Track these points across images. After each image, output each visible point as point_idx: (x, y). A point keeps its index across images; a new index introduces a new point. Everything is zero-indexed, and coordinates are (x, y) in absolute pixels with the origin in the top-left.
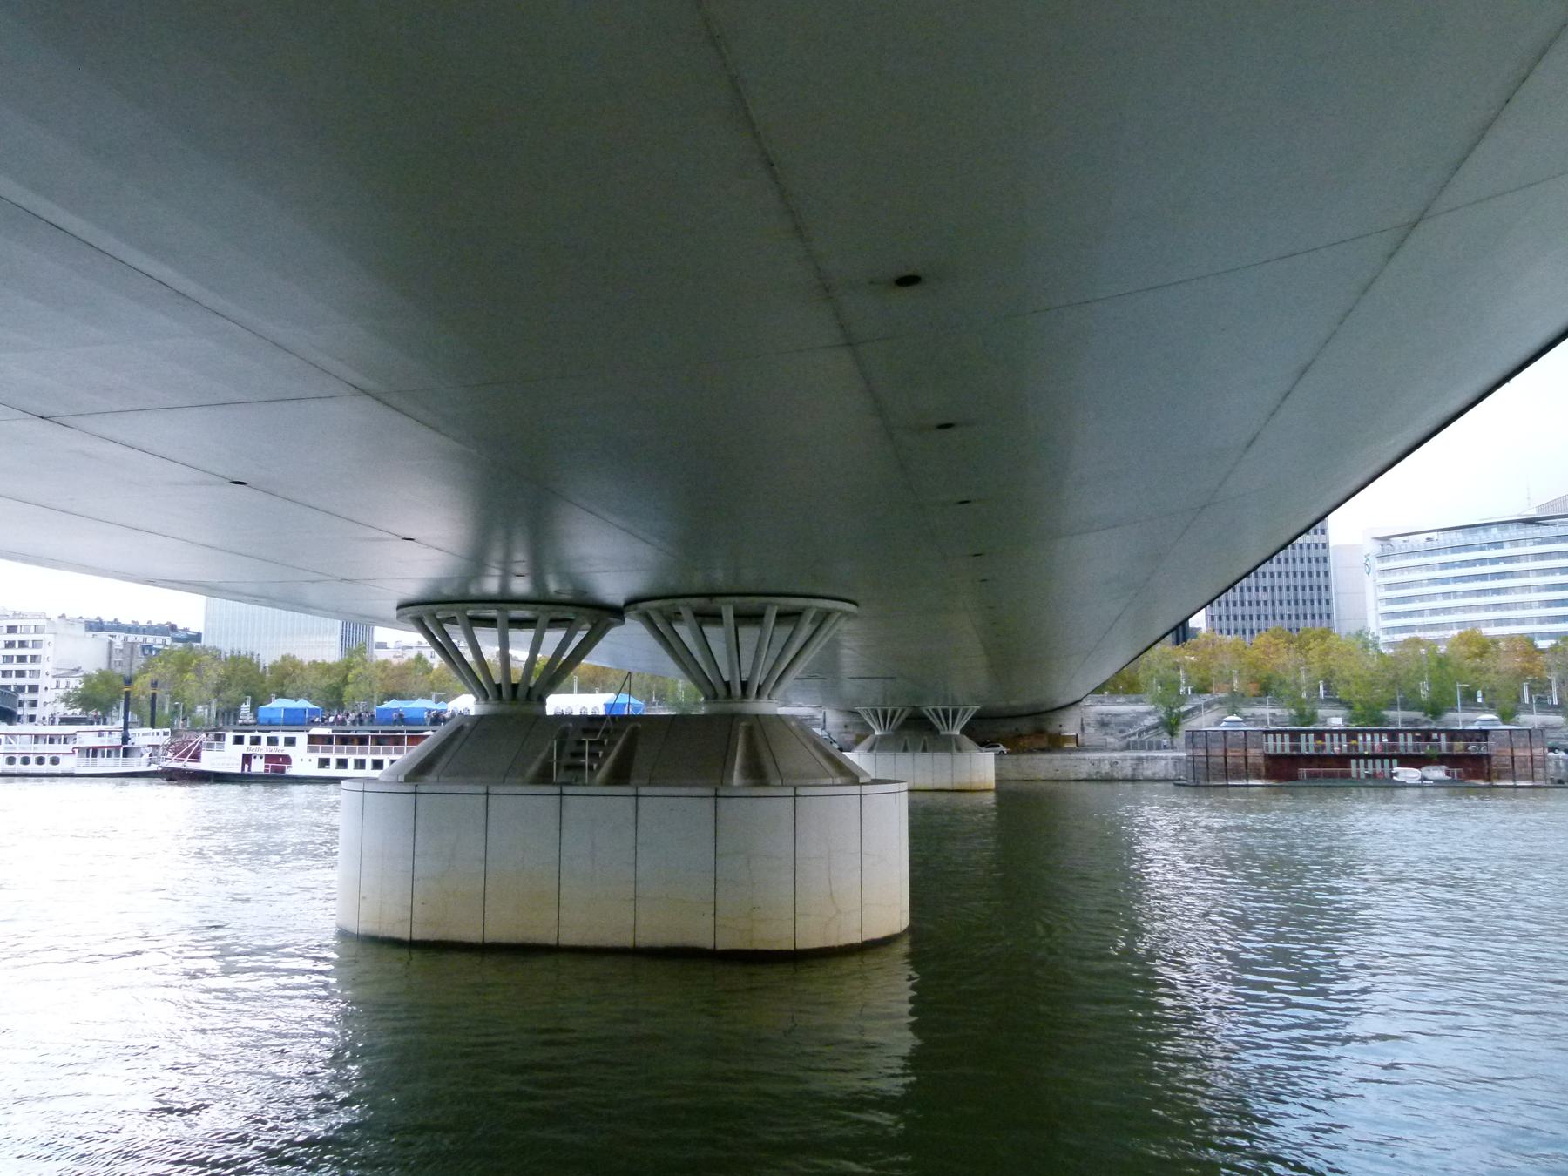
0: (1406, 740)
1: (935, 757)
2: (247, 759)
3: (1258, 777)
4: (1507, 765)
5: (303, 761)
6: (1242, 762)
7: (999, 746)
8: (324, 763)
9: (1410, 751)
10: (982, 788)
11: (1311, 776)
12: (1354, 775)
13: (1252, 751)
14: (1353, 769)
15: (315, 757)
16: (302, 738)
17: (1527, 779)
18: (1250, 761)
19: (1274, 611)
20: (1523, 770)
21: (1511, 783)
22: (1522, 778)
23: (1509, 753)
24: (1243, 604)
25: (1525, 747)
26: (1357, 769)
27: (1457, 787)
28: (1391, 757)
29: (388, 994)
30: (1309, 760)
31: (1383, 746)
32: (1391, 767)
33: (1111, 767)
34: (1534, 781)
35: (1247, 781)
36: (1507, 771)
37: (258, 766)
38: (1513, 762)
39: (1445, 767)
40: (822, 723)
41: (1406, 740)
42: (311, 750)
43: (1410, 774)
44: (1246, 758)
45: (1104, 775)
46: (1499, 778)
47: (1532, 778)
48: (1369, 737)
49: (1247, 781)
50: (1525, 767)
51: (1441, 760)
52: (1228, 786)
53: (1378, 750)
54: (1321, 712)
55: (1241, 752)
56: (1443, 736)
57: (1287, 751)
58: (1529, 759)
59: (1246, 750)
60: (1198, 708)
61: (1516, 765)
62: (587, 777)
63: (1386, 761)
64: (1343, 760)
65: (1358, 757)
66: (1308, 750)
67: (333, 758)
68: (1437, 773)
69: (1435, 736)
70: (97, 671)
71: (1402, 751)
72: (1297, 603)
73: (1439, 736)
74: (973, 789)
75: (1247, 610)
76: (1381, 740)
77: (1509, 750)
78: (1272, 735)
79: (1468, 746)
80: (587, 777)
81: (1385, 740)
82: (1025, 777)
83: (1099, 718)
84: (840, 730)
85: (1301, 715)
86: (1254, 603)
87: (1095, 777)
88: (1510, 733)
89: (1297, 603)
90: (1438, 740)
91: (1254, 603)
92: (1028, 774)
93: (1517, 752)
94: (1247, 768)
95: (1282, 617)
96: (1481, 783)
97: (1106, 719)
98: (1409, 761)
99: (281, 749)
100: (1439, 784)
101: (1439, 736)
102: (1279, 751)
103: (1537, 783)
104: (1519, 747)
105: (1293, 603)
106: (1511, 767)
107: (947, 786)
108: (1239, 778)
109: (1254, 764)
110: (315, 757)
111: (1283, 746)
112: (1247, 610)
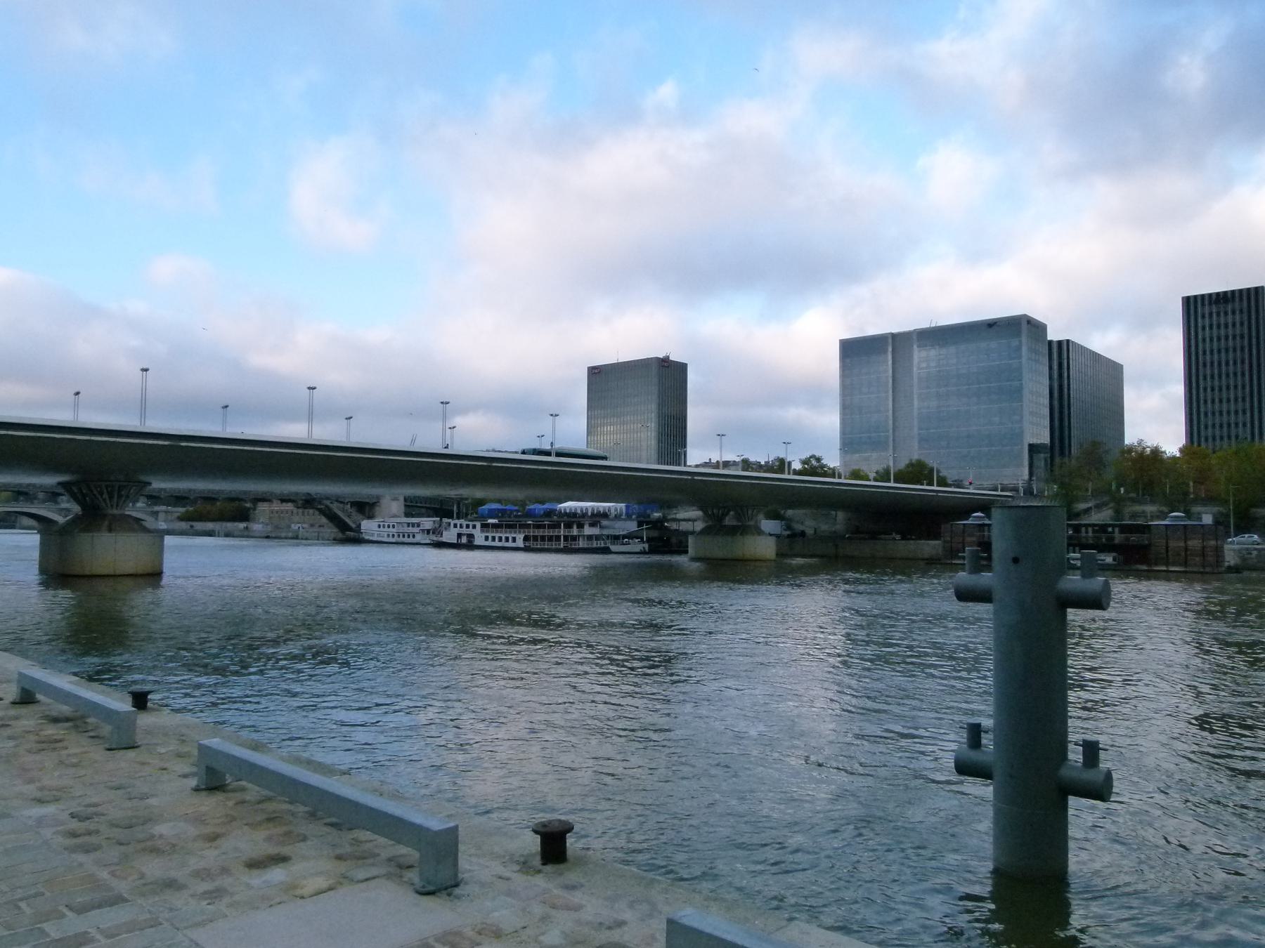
0: (1087, 532)
2: (459, 536)
5: (479, 539)
8: (487, 538)
10: (112, 572)
15: (484, 535)
16: (478, 525)
17: (1180, 565)
21: (1164, 568)
22: (1174, 564)
29: (560, 788)
37: (464, 540)
38: (1167, 551)
39: (1114, 554)
42: (482, 531)
46: (1156, 564)
47: (1185, 564)
50: (1179, 555)
52: (952, 564)
56: (1117, 530)
61: (1170, 553)
62: (1232, 530)
67: (490, 535)
70: (1152, 451)
74: (118, 572)
80: (1232, 530)
88: (1166, 529)
90: (1113, 532)
93: (1172, 544)
96: (1145, 568)
99: (470, 531)
101: (1113, 529)
110: (484, 535)
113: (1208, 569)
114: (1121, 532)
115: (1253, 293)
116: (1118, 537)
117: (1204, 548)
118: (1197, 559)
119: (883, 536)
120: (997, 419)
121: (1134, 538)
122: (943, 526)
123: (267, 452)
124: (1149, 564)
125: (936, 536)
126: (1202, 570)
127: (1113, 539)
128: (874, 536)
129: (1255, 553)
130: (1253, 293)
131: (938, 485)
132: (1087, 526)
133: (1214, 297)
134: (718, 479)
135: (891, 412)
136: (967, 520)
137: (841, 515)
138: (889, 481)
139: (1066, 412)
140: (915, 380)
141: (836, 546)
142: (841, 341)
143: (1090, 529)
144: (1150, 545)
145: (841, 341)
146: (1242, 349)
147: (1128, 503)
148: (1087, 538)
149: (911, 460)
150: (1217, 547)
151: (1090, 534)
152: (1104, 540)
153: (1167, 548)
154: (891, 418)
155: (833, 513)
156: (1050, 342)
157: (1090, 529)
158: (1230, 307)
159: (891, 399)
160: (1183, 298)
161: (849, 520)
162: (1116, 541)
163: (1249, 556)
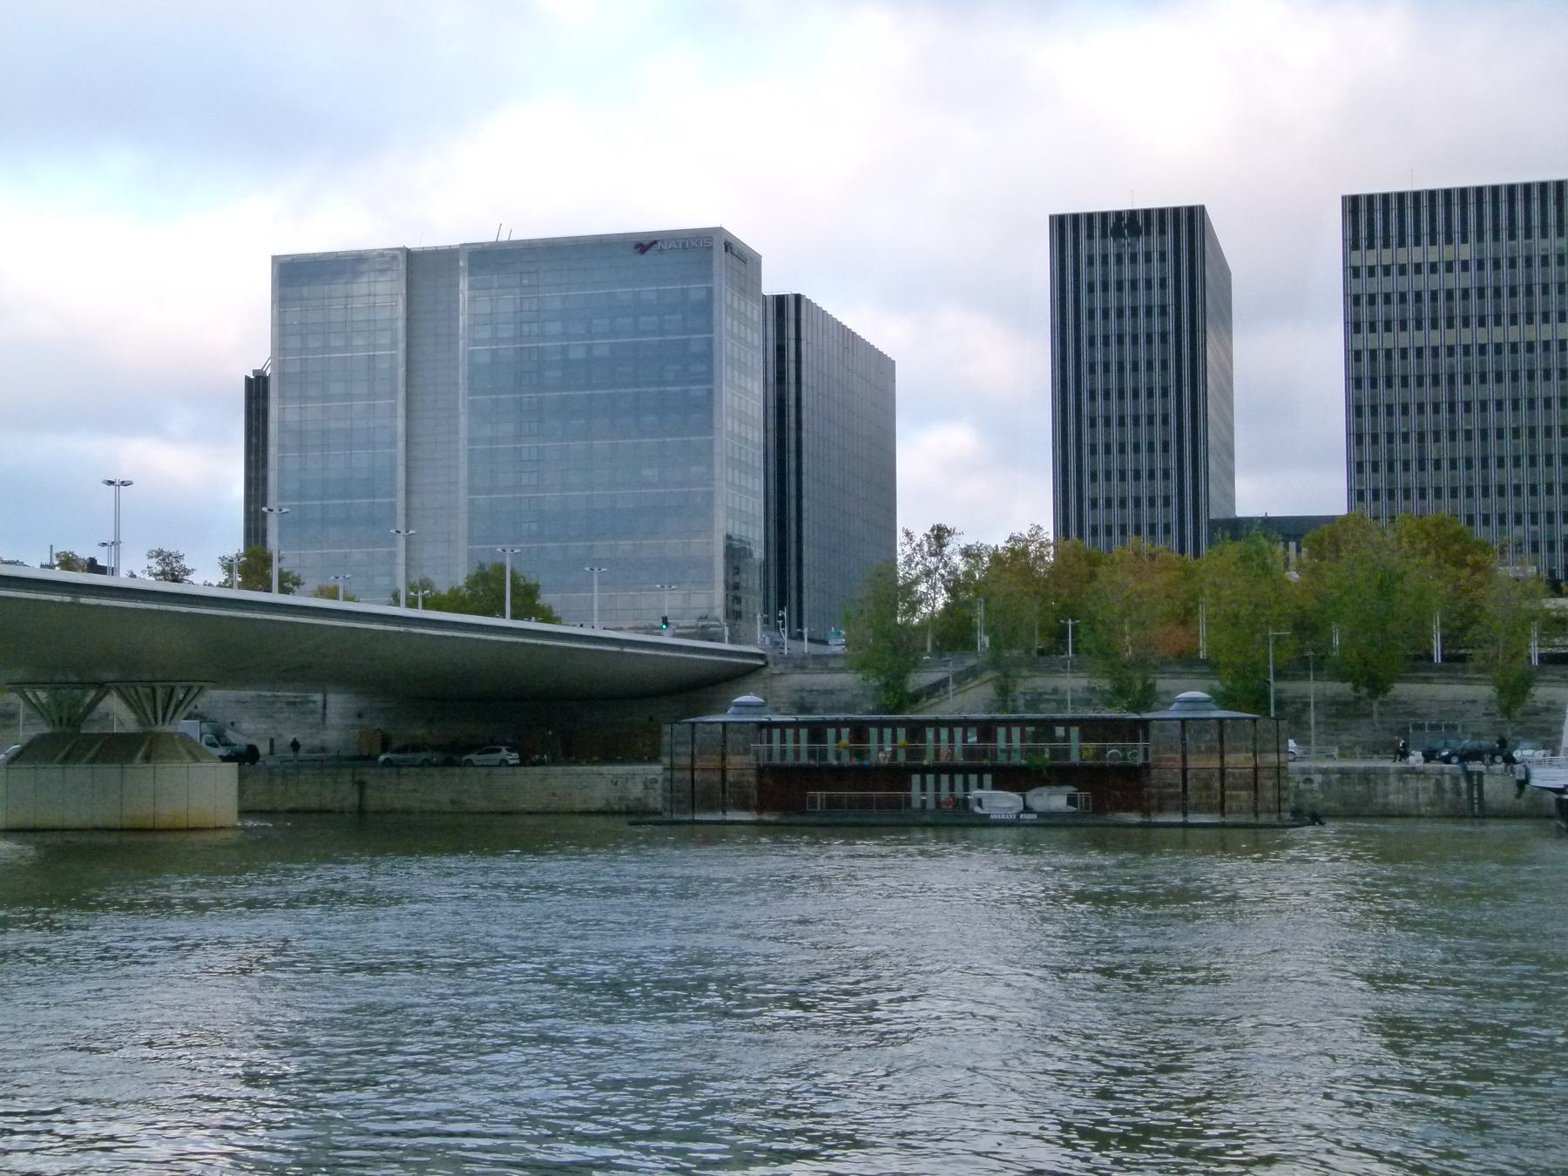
0: (1009, 739)
1: (69, 771)
3: (745, 807)
4: (1177, 786)
6: (716, 777)
7: (499, 751)
9: (1017, 760)
11: (832, 804)
12: (916, 804)
13: (735, 761)
14: (915, 791)
18: (730, 777)
19: (1485, 479)
20: (1204, 794)
22: (1197, 809)
23: (1180, 764)
24: (1422, 467)
25: (1210, 750)
26: (920, 793)
27: (1080, 826)
28: (980, 771)
30: (839, 775)
31: (969, 752)
32: (966, 788)
33: (646, 788)
34: (1223, 815)
35: (724, 812)
36: (1172, 797)
39: (1070, 789)
40: (320, 711)
41: (1009, 739)
43: (1001, 803)
44: (723, 771)
45: (631, 804)
46: (1161, 810)
47: (1222, 810)
48: (944, 733)
49: (724, 812)
50: (1208, 787)
51: (1059, 774)
52: (693, 822)
53: (960, 759)
54: (1163, 684)
55: (715, 761)
56: (1075, 732)
57: (804, 760)
58: (1217, 775)
59: (724, 758)
60: (942, 684)
63: (959, 779)
64: (896, 776)
65: (924, 771)
66: (838, 757)
68: (1055, 800)
69: (1060, 731)
71: (1002, 759)
72: (1533, 461)
73: (1067, 732)
75: (1430, 478)
76: (965, 740)
77: (1179, 756)
78: (833, 730)
79: (1105, 751)
81: (973, 739)
82: (500, 807)
83: (796, 697)
84: (350, 722)
85: (1120, 692)
86: (1445, 464)
87: (616, 807)
89: (1533, 461)
90: (1067, 738)
91: (1445, 464)
92: (505, 802)
93: (1193, 763)
94: (724, 792)
95: (1501, 491)
96: (1135, 818)
97: (809, 699)
98: (1012, 778)
100: (1050, 820)
101: (1067, 732)
102: (790, 760)
103: (1229, 819)
104: (1199, 752)
105: (1525, 461)
106: (1180, 790)
107: (114, 822)
108: (711, 809)
109: (737, 784)
111: (796, 750)
112: (1430, 478)
113: (1263, 819)
114: (1084, 737)
115: (1184, 217)
116: (1078, 750)
117: (1256, 769)
118: (1243, 793)
119: (473, 757)
120: (650, 473)
121: (1114, 752)
122: (667, 728)
123: (663, 657)
124: (1146, 812)
125: (654, 758)
126: (1253, 821)
127: (1067, 753)
128: (452, 754)
129: (1318, 778)
130: (1184, 217)
131: (514, 617)
132: (937, 724)
133: (1111, 221)
134: (515, 639)
135: (401, 445)
136: (724, 711)
137: (339, 705)
138: (495, 609)
139: (793, 464)
140: (463, 370)
141: (362, 785)
142: (276, 260)
143: (1016, 732)
144: (1146, 767)
145: (276, 260)
146: (1164, 337)
147: (1025, 672)
148: (1008, 751)
149: (482, 566)
150: (1278, 768)
151: (1016, 744)
152: (1047, 756)
153: (1184, 771)
154: (401, 460)
155: (318, 697)
156: (765, 297)
157: (1016, 732)
158: (1141, 246)
159: (401, 411)
160: (1051, 217)
161: (360, 716)
162: (1075, 758)
163: (1308, 786)
